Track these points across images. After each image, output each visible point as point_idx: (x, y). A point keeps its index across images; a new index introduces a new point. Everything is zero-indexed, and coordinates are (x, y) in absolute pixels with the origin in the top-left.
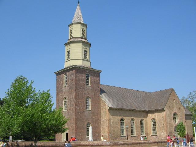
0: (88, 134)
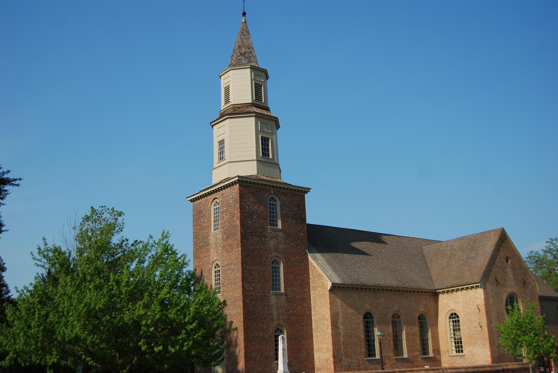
0: (277, 359)
